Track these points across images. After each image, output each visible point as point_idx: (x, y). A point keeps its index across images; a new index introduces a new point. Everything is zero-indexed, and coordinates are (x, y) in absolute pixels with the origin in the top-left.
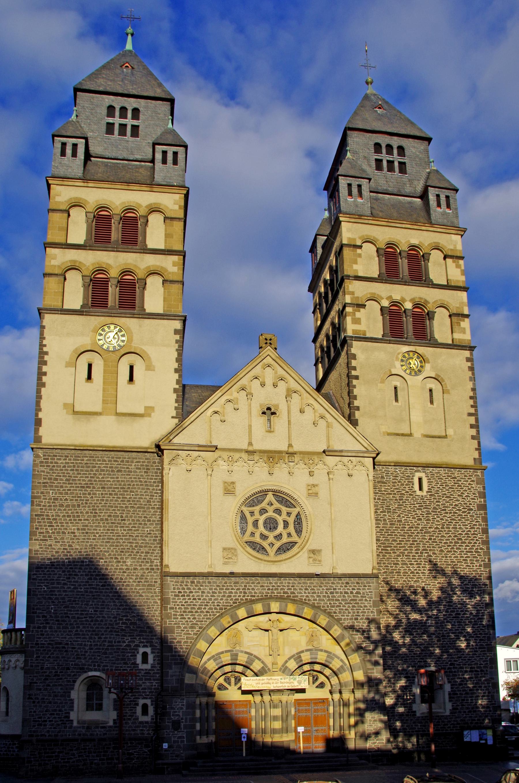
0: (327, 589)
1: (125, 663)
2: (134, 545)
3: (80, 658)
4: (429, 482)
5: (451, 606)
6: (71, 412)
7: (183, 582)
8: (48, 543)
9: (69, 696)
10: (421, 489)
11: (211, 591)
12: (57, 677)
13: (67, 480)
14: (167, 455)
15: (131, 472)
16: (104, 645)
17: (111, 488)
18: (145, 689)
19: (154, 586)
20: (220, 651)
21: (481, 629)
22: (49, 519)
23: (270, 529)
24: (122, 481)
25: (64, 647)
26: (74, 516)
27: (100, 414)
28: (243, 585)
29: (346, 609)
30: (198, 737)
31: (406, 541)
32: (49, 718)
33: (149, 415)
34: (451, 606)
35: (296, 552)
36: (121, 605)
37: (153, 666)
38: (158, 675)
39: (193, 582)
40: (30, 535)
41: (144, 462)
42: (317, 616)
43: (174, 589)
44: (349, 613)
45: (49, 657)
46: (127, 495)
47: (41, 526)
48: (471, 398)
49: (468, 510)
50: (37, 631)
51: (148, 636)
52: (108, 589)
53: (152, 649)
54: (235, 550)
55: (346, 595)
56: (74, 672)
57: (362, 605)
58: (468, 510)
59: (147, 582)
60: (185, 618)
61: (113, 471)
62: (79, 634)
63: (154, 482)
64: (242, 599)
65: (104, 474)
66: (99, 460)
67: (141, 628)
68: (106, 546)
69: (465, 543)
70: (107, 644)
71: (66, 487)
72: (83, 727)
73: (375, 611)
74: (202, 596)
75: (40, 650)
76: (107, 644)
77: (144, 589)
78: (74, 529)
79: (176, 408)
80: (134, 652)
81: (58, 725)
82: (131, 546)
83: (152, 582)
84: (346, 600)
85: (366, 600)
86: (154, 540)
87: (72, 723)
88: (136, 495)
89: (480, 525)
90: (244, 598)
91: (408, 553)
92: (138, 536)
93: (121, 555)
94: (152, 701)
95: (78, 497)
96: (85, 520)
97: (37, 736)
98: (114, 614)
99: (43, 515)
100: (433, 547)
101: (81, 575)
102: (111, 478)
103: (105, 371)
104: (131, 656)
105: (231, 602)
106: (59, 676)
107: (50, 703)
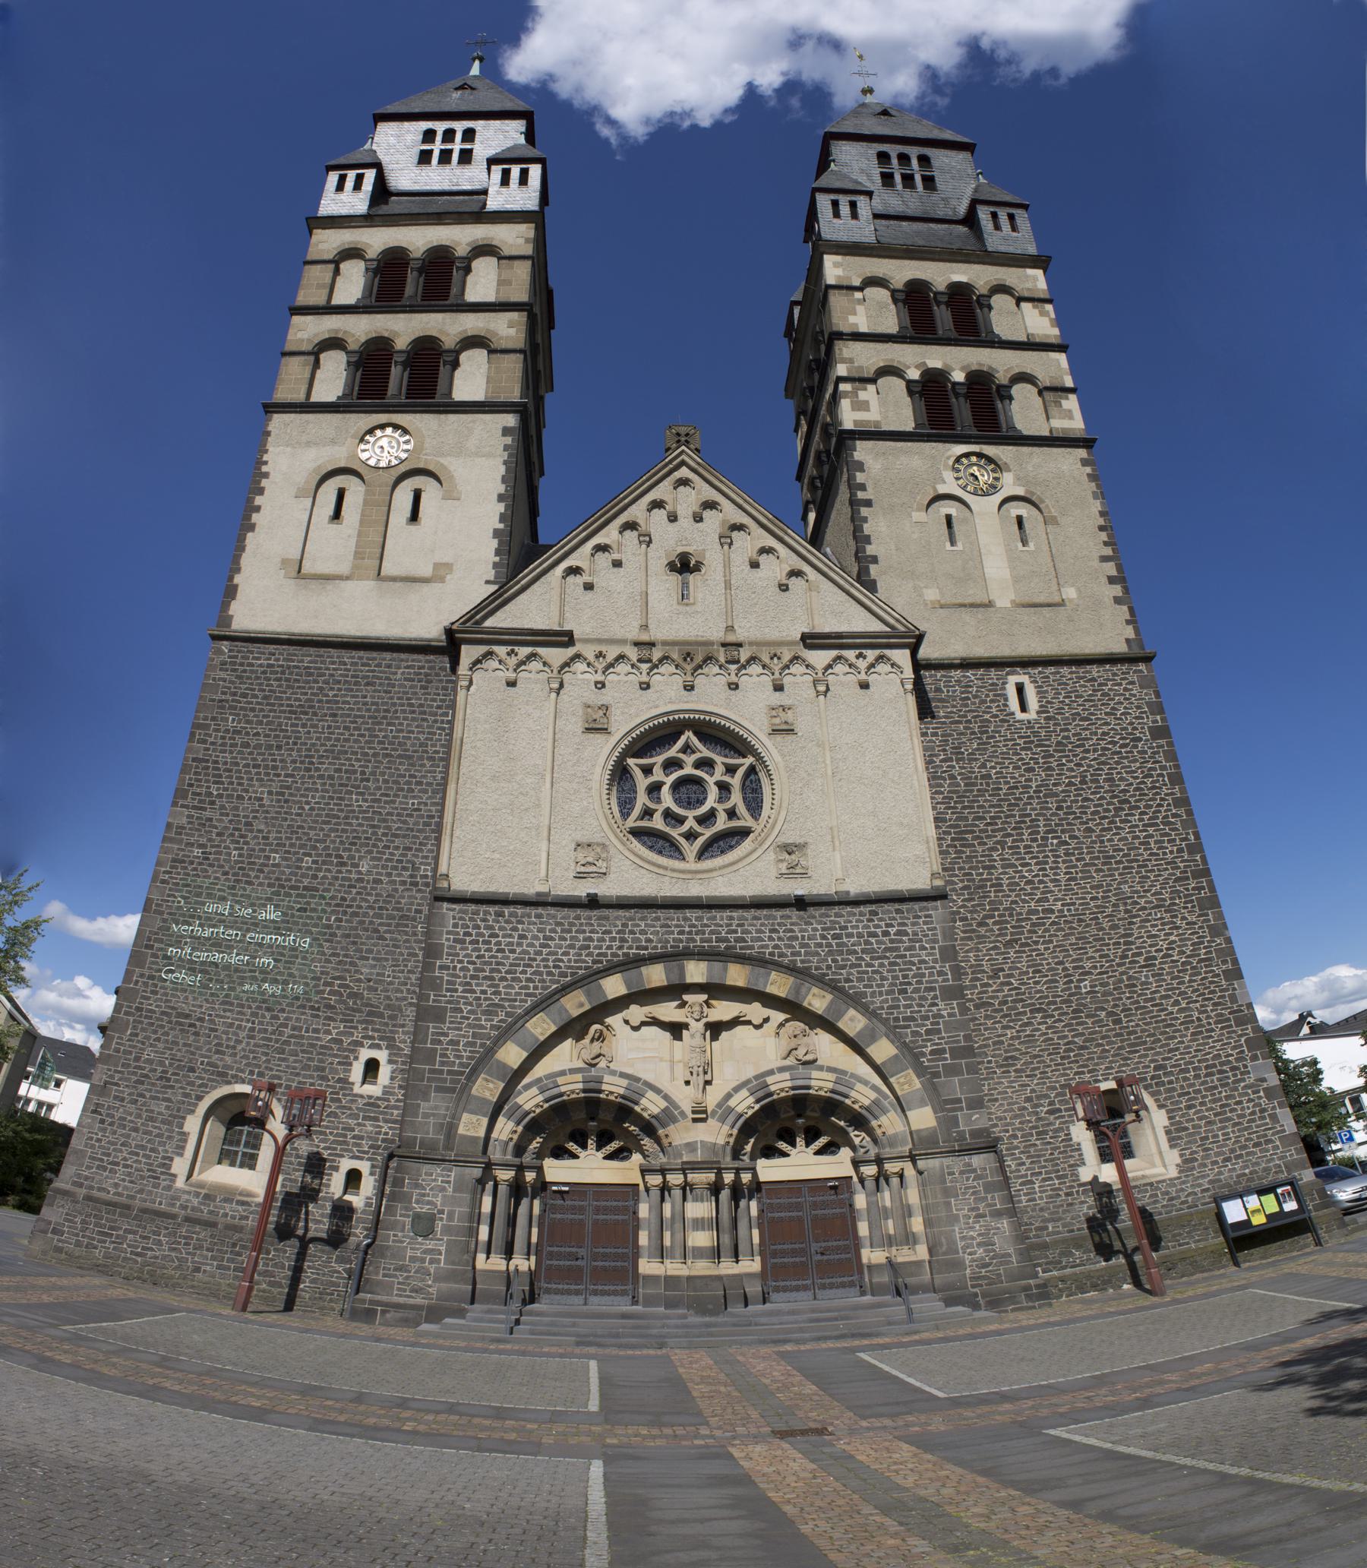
0: (823, 929)
1: (323, 1078)
2: (380, 832)
3: (223, 1053)
4: (1041, 693)
5: (1132, 943)
6: (294, 574)
7: (477, 913)
8: (207, 814)
9: (181, 1126)
10: (1024, 708)
11: (541, 935)
12: (164, 1083)
13: (265, 697)
14: (468, 654)
15: (393, 686)
16: (281, 1034)
17: (349, 716)
18: (361, 1138)
19: (414, 919)
20: (557, 1068)
21: (1211, 982)
22: (218, 769)
23: (689, 803)
24: (373, 704)
25: (194, 1025)
26: (266, 767)
27: (347, 578)
28: (619, 923)
29: (874, 972)
30: (481, 1257)
31: (1007, 817)
32: (125, 1159)
33: (442, 580)
34: (1132, 943)
35: (750, 848)
36: (333, 955)
37: (387, 1091)
38: (396, 1112)
39: (500, 914)
40: (175, 797)
41: (423, 667)
42: (803, 990)
43: (455, 925)
44: (883, 979)
45: (158, 1040)
46: (380, 730)
47: (200, 780)
48: (1101, 528)
49: (1132, 740)
50: (146, 984)
51: (387, 1024)
52: (312, 918)
53: (390, 1055)
54: (604, 846)
55: (873, 940)
56: (202, 1078)
57: (915, 960)
58: (1132, 740)
59: (398, 909)
60: (474, 992)
61: (356, 683)
62: (232, 1004)
63: (439, 707)
64: (614, 955)
65: (340, 690)
66: (333, 663)
67: (372, 1006)
68: (322, 829)
69: (1139, 808)
70: (288, 1031)
71: (262, 710)
72: (197, 1195)
73: (947, 968)
74: (519, 944)
75: (141, 1022)
76: (288, 1031)
77: (389, 925)
78: (262, 793)
79: (495, 565)
80: (347, 1057)
81: (142, 1178)
82: (375, 833)
83: (409, 910)
84: (874, 951)
85: (923, 948)
86: (426, 824)
87: (174, 1181)
88: (399, 731)
89: (1163, 768)
90: (620, 953)
91: (1014, 841)
92: (391, 814)
93: (350, 850)
94: (373, 1166)
95: (282, 731)
96: (287, 775)
97: (91, 1188)
98: (314, 972)
99: (207, 761)
100: (1068, 824)
101: (260, 884)
102: (353, 696)
103: (366, 503)
104: (339, 1063)
105: (589, 959)
106: (168, 1080)
107: (136, 1130)
